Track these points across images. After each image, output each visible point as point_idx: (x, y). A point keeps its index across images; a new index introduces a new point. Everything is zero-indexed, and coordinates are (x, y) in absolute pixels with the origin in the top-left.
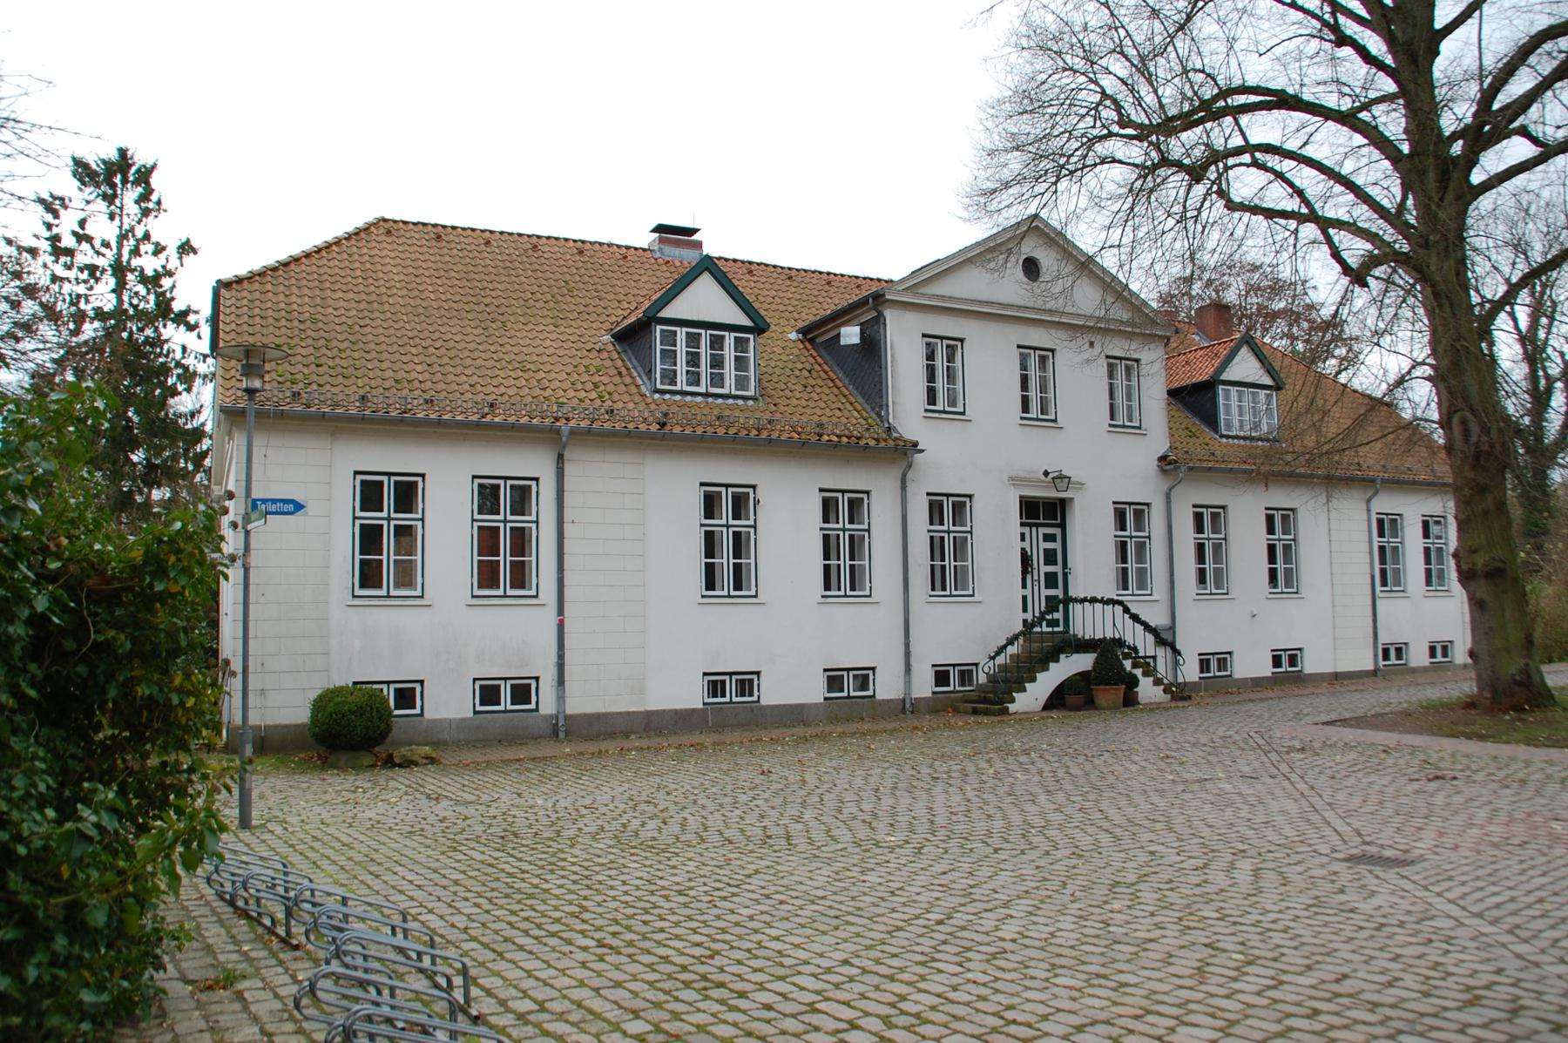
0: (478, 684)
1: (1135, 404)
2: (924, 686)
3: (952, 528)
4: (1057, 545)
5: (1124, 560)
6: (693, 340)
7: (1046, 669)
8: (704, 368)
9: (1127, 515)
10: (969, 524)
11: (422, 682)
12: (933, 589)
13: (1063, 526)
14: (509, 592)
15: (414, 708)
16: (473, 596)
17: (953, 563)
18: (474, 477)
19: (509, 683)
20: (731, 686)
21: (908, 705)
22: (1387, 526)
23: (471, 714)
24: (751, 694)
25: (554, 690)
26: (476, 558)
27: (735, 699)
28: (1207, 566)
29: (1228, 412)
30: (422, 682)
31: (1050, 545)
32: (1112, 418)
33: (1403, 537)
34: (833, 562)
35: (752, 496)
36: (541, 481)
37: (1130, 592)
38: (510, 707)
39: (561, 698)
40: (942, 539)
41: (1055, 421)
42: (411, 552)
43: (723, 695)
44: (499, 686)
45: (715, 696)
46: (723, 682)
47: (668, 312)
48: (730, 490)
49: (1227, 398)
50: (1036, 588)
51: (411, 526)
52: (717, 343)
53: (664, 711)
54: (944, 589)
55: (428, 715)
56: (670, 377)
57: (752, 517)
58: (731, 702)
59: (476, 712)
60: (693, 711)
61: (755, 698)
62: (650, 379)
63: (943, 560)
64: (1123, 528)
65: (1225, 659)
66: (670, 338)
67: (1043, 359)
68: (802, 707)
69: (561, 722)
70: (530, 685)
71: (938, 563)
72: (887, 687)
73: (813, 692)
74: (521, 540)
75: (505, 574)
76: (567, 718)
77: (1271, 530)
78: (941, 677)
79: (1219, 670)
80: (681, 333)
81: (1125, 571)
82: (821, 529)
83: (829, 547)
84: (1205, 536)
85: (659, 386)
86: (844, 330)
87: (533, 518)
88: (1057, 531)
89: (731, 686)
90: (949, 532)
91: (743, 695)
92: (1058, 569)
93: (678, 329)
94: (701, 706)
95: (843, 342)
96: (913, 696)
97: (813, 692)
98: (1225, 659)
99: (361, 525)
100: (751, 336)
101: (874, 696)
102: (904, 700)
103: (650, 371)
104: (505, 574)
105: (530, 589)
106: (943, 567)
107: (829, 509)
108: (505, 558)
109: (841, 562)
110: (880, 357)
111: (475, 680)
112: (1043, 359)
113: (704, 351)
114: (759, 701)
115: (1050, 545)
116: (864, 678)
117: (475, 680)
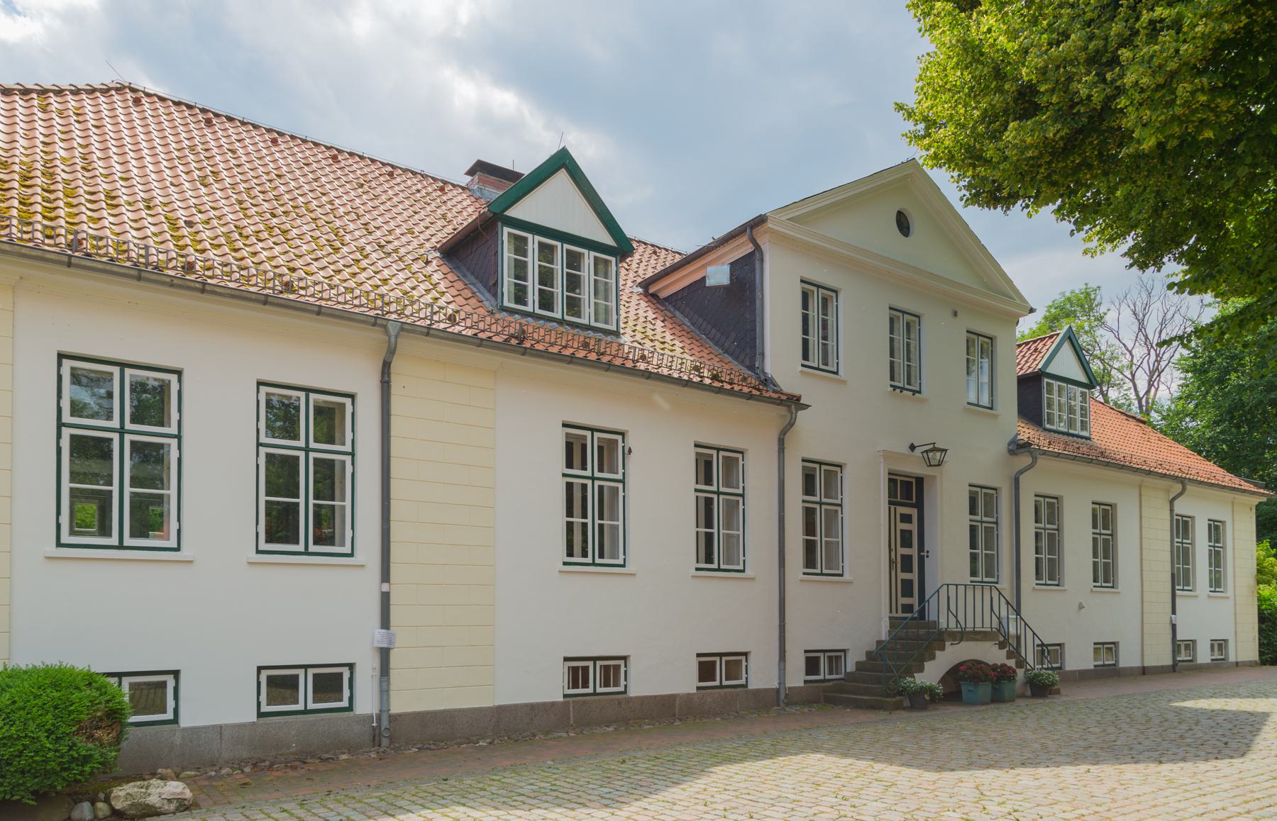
0: (264, 674)
1: (914, 364)
2: (796, 677)
3: (597, 474)
4: (913, 527)
5: (709, 524)
6: (574, 261)
7: (933, 657)
8: (559, 290)
9: (982, 500)
10: (621, 470)
11: (176, 674)
12: (570, 554)
13: (920, 506)
14: (312, 548)
15: (715, 680)
16: (258, 552)
17: (597, 522)
18: (260, 384)
19: (311, 672)
20: (595, 674)
21: (782, 696)
22: (1182, 527)
23: (253, 717)
24: (616, 684)
25: (377, 680)
26: (263, 498)
27: (599, 690)
28: (818, 538)
29: (1049, 406)
30: (176, 674)
31: (906, 526)
32: (892, 378)
33: (1193, 539)
34: (577, 520)
35: (620, 444)
36: (359, 399)
37: (715, 566)
38: (311, 706)
39: (384, 692)
40: (584, 487)
41: (836, 373)
42: (159, 481)
43: (585, 685)
44: (297, 677)
45: (575, 686)
46: (586, 669)
47: (515, 212)
48: (597, 435)
49: (1050, 392)
50: (893, 573)
51: (161, 446)
52: (574, 261)
53: (516, 707)
54: (585, 555)
55: (185, 722)
56: (520, 296)
57: (621, 470)
58: (595, 694)
59: (260, 715)
60: (553, 704)
61: (621, 689)
62: (495, 295)
63: (584, 516)
64: (708, 481)
65: (617, 668)
66: (520, 246)
67: (825, 301)
68: (671, 698)
69: (385, 723)
70: (341, 675)
71: (577, 520)
72: (760, 676)
73: (685, 682)
74: (328, 476)
75: (122, 514)
76: (394, 718)
77: (973, 510)
78: (812, 665)
79: (831, 673)
80: (533, 242)
81: (709, 537)
82: (564, 475)
83: (573, 500)
84: (817, 499)
85: (506, 303)
86: (710, 269)
87: (173, 430)
88: (914, 512)
89: (595, 674)
90: (593, 479)
91: (607, 684)
92: (914, 551)
93: (529, 236)
94: (561, 699)
95: (709, 283)
96: (787, 686)
97: (685, 682)
98: (838, 658)
99: (73, 437)
100: (613, 259)
101: (745, 686)
102: (778, 691)
103: (496, 284)
104: (122, 514)
105: (343, 545)
106: (584, 525)
107: (574, 452)
108: (306, 502)
109: (589, 521)
110: (753, 302)
111: (260, 669)
112: (825, 301)
113: (559, 267)
114: (625, 692)
115: (906, 526)
116: (735, 662)
117: (260, 669)
